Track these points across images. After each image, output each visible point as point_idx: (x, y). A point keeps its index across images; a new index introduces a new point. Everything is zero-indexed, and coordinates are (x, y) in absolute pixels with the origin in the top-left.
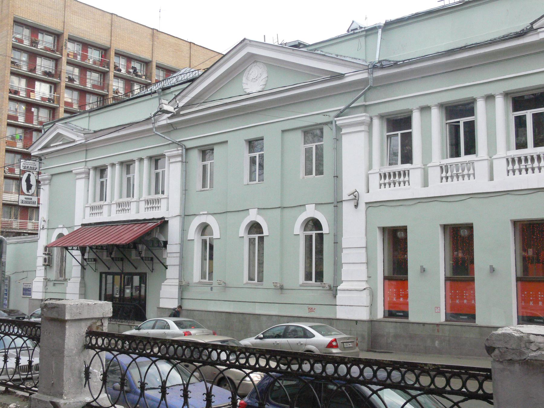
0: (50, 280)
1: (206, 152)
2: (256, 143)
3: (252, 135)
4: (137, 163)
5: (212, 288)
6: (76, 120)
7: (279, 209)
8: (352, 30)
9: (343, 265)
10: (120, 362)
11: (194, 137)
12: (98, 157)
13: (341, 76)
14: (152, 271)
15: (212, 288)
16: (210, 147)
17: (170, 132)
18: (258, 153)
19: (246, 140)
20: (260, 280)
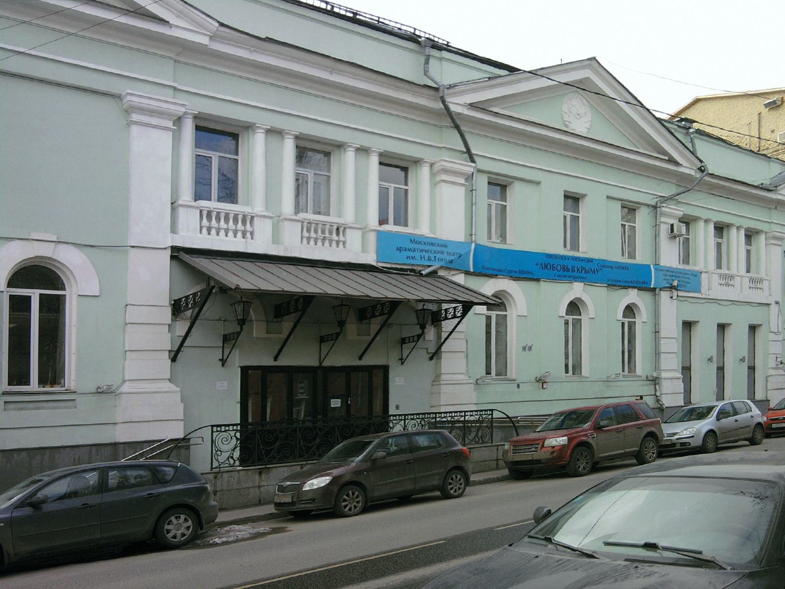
0: (140, 386)
1: (500, 186)
2: (310, 153)
3: (575, 187)
4: (350, 156)
5: (518, 386)
6: (388, 43)
7: (54, 243)
8: (682, 120)
9: (442, 353)
10: (770, 478)
11: (494, 156)
12: (227, 99)
13: (677, 164)
14: (402, 361)
15: (518, 386)
16: (327, 149)
17: (441, 127)
18: (393, 185)
19: (584, 196)
20: (52, 373)
